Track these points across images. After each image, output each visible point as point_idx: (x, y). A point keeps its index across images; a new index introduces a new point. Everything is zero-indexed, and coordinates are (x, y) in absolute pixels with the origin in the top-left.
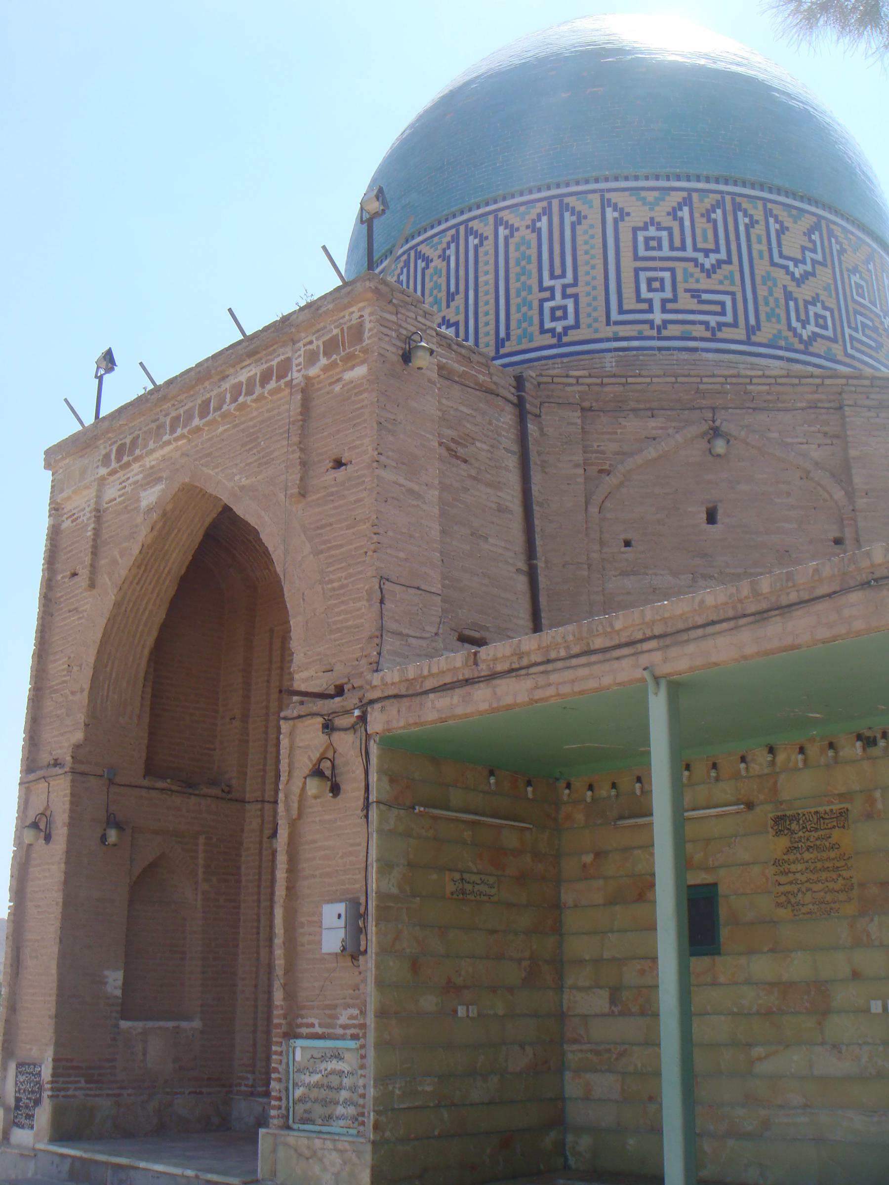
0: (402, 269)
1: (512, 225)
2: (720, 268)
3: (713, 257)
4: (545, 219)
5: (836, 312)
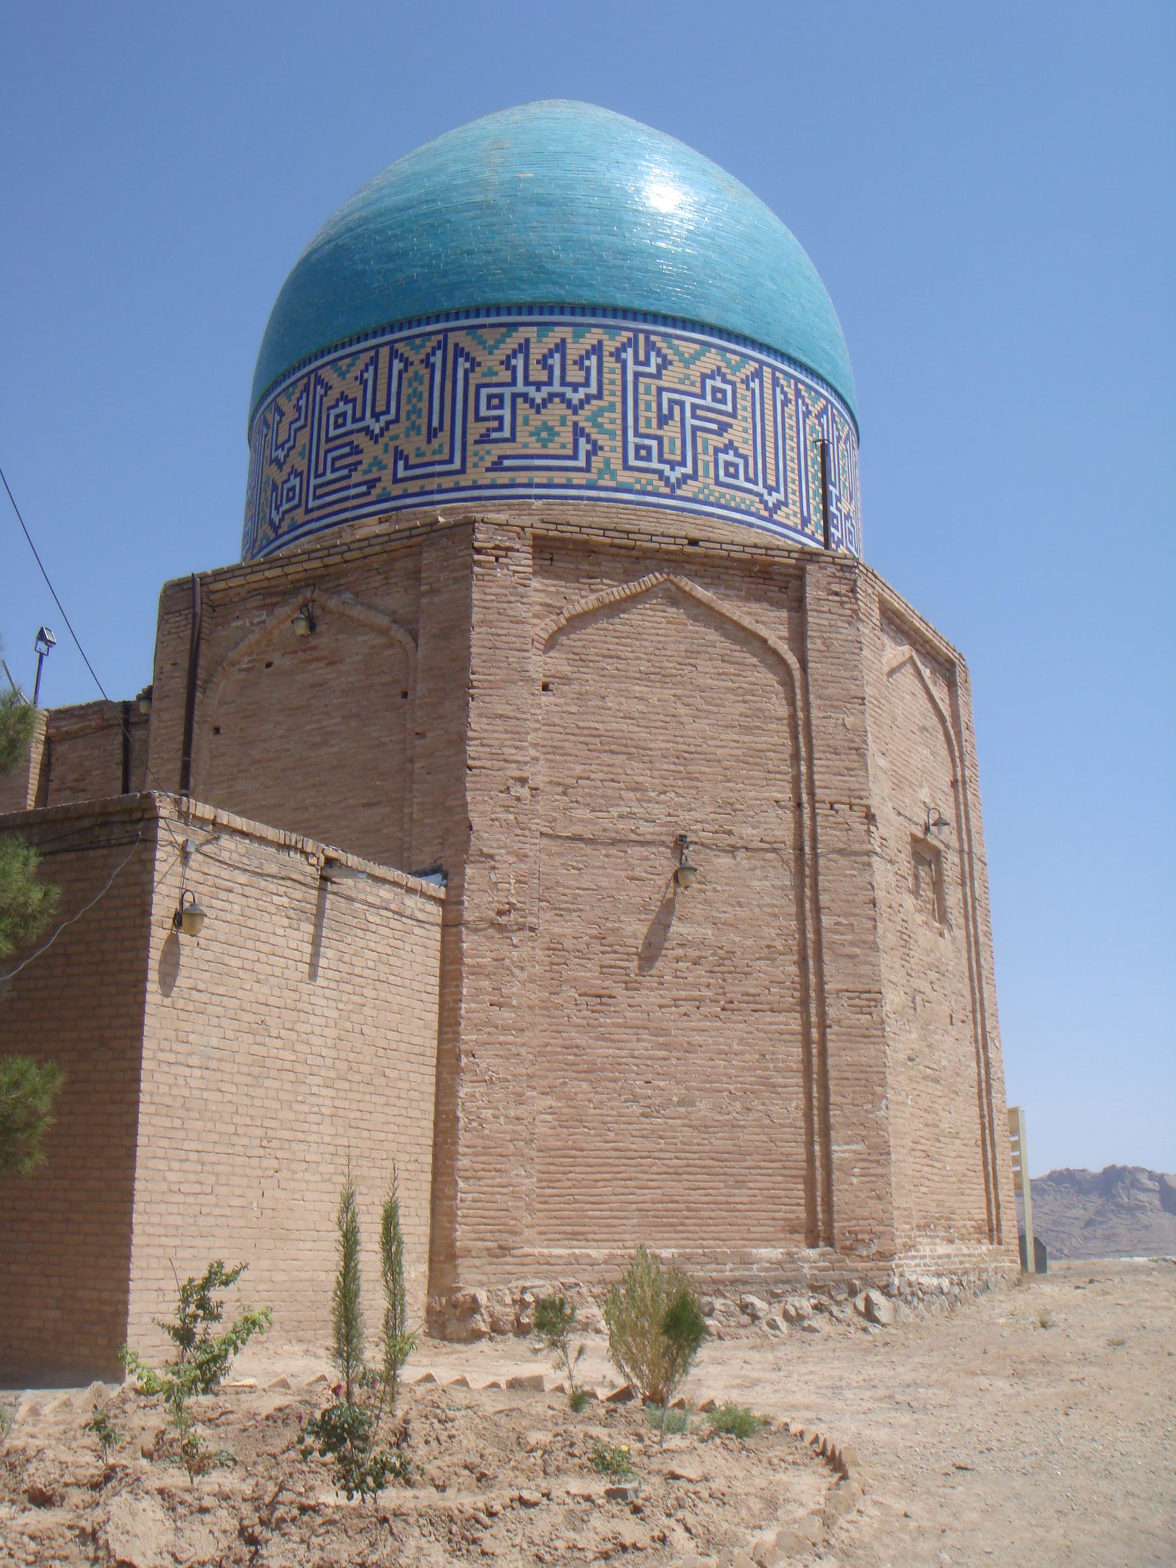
0: (367, 366)
1: (407, 359)
2: (685, 483)
3: (680, 471)
4: (439, 353)
5: (751, 460)
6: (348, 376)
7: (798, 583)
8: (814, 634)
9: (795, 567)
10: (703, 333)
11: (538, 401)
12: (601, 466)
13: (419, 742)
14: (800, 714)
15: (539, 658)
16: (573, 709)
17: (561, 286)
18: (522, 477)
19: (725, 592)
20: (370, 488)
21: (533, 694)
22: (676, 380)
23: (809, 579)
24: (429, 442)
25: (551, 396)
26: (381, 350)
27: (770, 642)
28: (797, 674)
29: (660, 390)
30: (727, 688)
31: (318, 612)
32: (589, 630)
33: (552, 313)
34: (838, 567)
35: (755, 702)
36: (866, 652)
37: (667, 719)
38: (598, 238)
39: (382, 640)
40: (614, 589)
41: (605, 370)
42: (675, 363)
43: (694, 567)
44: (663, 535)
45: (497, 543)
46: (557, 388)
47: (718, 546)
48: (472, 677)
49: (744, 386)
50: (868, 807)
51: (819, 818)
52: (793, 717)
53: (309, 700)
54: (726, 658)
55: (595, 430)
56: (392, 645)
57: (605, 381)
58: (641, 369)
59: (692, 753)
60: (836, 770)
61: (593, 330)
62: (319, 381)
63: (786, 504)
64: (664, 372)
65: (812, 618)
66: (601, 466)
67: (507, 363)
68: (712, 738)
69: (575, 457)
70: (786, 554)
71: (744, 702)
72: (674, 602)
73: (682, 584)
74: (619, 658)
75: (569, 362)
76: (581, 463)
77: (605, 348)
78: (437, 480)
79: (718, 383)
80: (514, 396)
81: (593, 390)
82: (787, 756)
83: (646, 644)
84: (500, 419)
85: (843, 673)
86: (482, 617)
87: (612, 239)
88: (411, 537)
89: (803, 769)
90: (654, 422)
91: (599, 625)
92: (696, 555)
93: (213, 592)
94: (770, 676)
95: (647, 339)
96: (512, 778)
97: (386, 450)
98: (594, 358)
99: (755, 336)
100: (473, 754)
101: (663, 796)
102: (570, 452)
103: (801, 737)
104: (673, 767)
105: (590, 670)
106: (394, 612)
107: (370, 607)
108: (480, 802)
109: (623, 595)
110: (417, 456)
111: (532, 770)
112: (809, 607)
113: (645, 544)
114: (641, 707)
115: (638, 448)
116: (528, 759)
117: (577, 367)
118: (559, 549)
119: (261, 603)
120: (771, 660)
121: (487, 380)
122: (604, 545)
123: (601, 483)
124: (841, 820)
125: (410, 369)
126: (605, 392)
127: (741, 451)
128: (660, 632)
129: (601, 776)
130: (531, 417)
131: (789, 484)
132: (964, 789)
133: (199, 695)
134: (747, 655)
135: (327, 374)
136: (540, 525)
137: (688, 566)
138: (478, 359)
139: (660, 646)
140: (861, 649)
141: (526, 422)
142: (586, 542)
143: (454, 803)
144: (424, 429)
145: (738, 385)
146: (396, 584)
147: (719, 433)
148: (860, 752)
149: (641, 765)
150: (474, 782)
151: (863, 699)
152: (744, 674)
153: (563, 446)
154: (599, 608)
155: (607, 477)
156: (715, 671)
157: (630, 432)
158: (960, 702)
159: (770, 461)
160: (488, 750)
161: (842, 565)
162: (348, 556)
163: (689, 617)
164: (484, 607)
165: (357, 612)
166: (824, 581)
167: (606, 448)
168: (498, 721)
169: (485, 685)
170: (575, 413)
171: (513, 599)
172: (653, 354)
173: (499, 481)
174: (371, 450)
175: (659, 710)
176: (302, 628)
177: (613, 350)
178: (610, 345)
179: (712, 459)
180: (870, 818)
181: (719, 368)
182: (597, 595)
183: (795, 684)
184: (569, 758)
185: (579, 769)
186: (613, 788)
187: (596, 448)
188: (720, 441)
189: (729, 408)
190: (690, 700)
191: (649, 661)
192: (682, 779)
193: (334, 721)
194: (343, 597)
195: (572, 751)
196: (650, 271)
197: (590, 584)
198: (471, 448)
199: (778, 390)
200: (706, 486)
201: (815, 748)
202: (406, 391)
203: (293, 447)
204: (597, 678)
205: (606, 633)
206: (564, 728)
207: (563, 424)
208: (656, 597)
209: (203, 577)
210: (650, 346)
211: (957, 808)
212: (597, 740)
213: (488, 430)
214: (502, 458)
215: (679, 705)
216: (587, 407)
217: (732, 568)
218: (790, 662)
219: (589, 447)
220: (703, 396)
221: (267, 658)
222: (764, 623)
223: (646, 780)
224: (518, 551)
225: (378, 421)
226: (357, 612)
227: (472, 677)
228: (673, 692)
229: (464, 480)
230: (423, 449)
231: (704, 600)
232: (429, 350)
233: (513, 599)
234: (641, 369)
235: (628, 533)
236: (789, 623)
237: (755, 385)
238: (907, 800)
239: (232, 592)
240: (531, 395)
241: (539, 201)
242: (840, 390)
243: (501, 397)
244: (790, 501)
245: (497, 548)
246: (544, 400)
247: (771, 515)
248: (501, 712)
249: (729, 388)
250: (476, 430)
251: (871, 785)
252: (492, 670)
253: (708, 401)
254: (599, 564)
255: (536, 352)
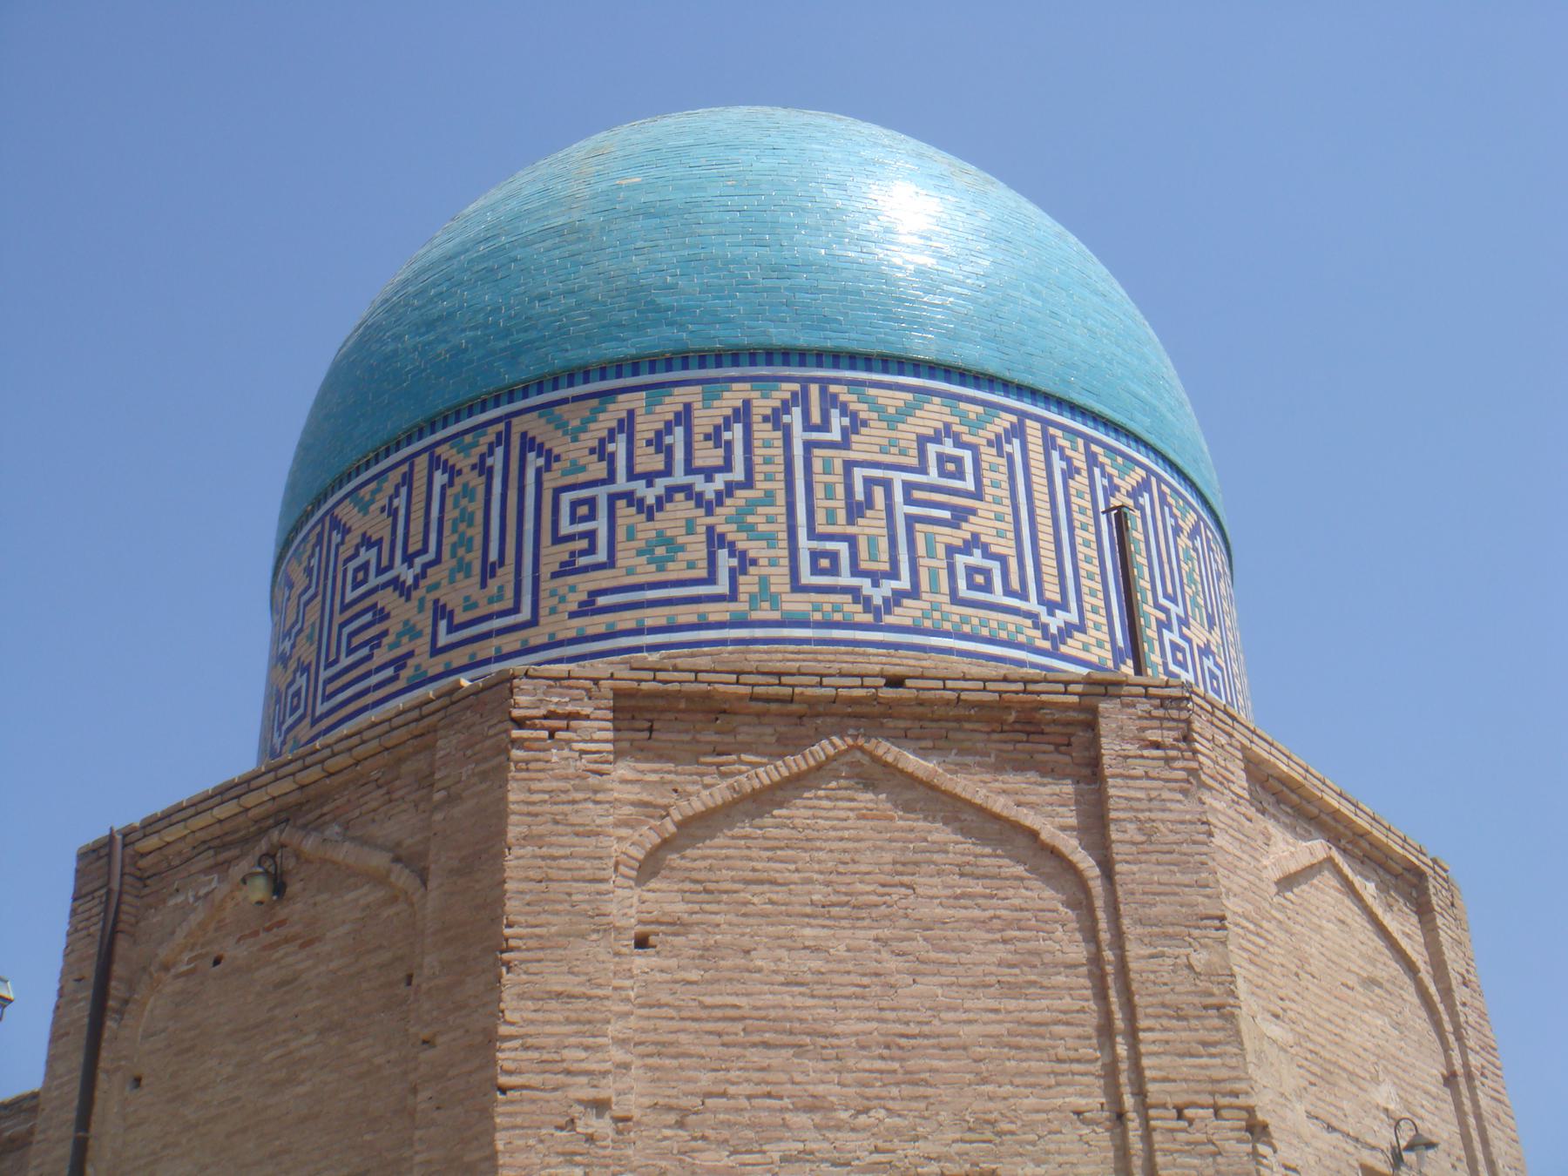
0: (397, 488)
3: (888, 586)
4: (499, 451)
5: (1013, 564)
6: (373, 507)
7: (1089, 735)
8: (1121, 815)
9: (1078, 708)
10: (917, 375)
11: (651, 500)
12: (755, 589)
13: (427, 1055)
14: (1108, 955)
15: (627, 892)
16: (694, 975)
17: (682, 327)
18: (627, 620)
19: (959, 759)
20: (398, 669)
21: (617, 954)
22: (877, 449)
23: (1105, 726)
24: (484, 585)
25: (671, 491)
26: (418, 460)
27: (1044, 836)
28: (1097, 887)
29: (849, 465)
30: (972, 920)
31: (291, 863)
32: (718, 841)
33: (669, 368)
34: (1157, 702)
35: (1027, 940)
36: (1219, 840)
37: (866, 981)
38: (739, 251)
39: (380, 894)
40: (761, 770)
41: (756, 443)
42: (872, 423)
43: (902, 724)
44: (842, 675)
45: (552, 707)
46: (679, 477)
47: (940, 684)
48: (507, 932)
49: (994, 451)
50: (1250, 1110)
51: (1157, 1137)
52: (1096, 960)
53: (271, 1009)
54: (967, 869)
55: (743, 535)
56: (394, 900)
57: (757, 460)
58: (815, 436)
59: (914, 1037)
60: (1181, 1047)
61: (735, 386)
62: (336, 524)
63: (1082, 628)
64: (854, 438)
65: (1115, 789)
66: (755, 589)
67: (600, 451)
68: (949, 1009)
69: (711, 579)
70: (1061, 687)
71: (1005, 942)
72: (869, 784)
73: (880, 752)
74: (773, 882)
75: (698, 437)
76: (723, 587)
77: (755, 410)
78: (495, 641)
79: (948, 448)
80: (613, 498)
81: (738, 474)
82: (1090, 1031)
83: (822, 855)
84: (591, 535)
85: (1179, 877)
86: (524, 829)
87: (762, 251)
88: (422, 717)
89: (1122, 1050)
90: (842, 515)
91: (736, 831)
92: (900, 702)
93: (143, 855)
94: (1048, 893)
95: (823, 391)
96: (580, 1102)
97: (421, 609)
98: (738, 428)
99: (1007, 375)
100: (508, 1065)
101: (862, 1119)
102: (703, 573)
103: (1112, 993)
104: (879, 1064)
105: (723, 907)
106: (399, 844)
107: (365, 842)
108: (519, 1150)
109: (776, 777)
110: (466, 609)
111: (620, 1086)
112: (1107, 772)
113: (809, 691)
114: (816, 964)
115: (815, 556)
116: (608, 1066)
117: (711, 444)
118: (663, 711)
119: (210, 862)
120: (1049, 866)
121: (571, 480)
122: (740, 698)
123: (756, 615)
124: (1200, 1137)
125: (457, 480)
126: (758, 477)
127: (994, 549)
128: (846, 834)
129: (748, 1089)
130: (640, 527)
131: (1086, 598)
132: (1472, 1090)
133: (110, 1024)
134: (1006, 861)
135: (348, 513)
136: (627, 674)
137: (890, 723)
138: (556, 451)
139: (847, 857)
140: (1211, 835)
141: (631, 536)
142: (707, 696)
143: (477, 1155)
144: (477, 568)
145: (983, 449)
146: (403, 798)
147: (955, 523)
148: (1226, 1013)
149: (821, 1065)
150: (510, 1114)
151: (1222, 918)
152: (1001, 893)
153: (691, 565)
154: (735, 803)
155: (766, 605)
156: (949, 892)
157: (802, 533)
158: (1443, 937)
159: (1049, 564)
160: (536, 1055)
161: (1162, 698)
162: (333, 764)
163: (896, 806)
164: (529, 814)
165: (346, 853)
166: (1132, 727)
167: (763, 562)
168: (553, 1004)
169: (532, 943)
170: (709, 513)
171: (579, 796)
172: (835, 413)
173: (591, 631)
174: (400, 610)
175: (850, 967)
176: (259, 890)
177: (769, 412)
178: (762, 406)
179: (944, 564)
180: (1257, 1130)
181: (947, 426)
182: (730, 781)
183: (1093, 903)
184: (687, 1061)
185: (705, 1080)
186: (769, 1109)
187: (745, 562)
188: (957, 537)
189: (969, 484)
190: (905, 946)
191: (828, 884)
192: (897, 1084)
193: (306, 1040)
194: (327, 833)
195: (692, 1050)
196: (822, 291)
197: (719, 765)
198: (546, 585)
199: (1055, 455)
200: (935, 607)
201: (1140, 1012)
202: (451, 514)
203: (301, 630)
204: (735, 920)
205: (750, 842)
206: (678, 1008)
207: (690, 531)
208: (837, 778)
209: (127, 833)
210: (829, 401)
211: (1463, 1124)
212: (740, 1026)
213: (572, 554)
214: (594, 594)
215: (885, 955)
216: (728, 501)
217: (969, 719)
218: (1082, 866)
219: (734, 562)
220: (923, 470)
221: (215, 950)
222: (1031, 806)
223: (831, 1091)
224: (587, 717)
225: (411, 566)
226: (346, 853)
227: (507, 932)
228: (873, 933)
229: (536, 636)
230: (474, 598)
231: (920, 774)
232: (484, 449)
233: (579, 796)
234: (815, 436)
235: (779, 674)
236: (1077, 803)
237: (1014, 447)
238: (1345, 1104)
239: (170, 851)
240: (639, 494)
241: (647, 212)
242: (1172, 456)
243: (591, 502)
244: (1090, 624)
245: (551, 715)
246: (659, 499)
247: (1055, 646)
248: (559, 988)
249: (967, 455)
250: (554, 556)
251: (1251, 1069)
252: (543, 918)
253: (933, 476)
254: (733, 731)
255: (645, 428)
